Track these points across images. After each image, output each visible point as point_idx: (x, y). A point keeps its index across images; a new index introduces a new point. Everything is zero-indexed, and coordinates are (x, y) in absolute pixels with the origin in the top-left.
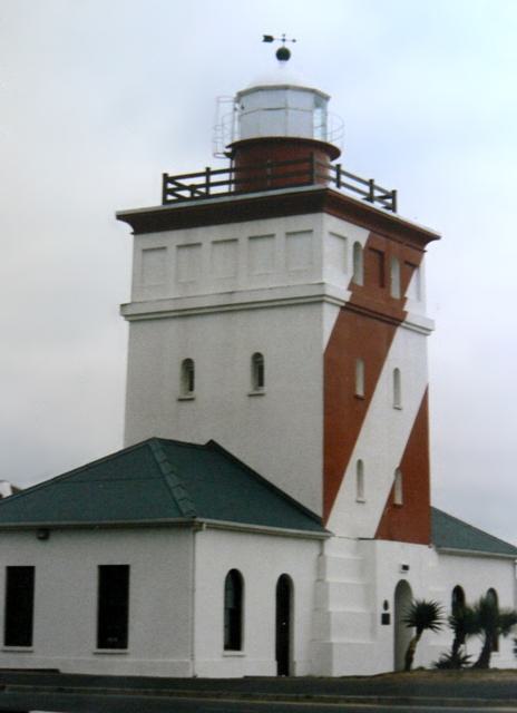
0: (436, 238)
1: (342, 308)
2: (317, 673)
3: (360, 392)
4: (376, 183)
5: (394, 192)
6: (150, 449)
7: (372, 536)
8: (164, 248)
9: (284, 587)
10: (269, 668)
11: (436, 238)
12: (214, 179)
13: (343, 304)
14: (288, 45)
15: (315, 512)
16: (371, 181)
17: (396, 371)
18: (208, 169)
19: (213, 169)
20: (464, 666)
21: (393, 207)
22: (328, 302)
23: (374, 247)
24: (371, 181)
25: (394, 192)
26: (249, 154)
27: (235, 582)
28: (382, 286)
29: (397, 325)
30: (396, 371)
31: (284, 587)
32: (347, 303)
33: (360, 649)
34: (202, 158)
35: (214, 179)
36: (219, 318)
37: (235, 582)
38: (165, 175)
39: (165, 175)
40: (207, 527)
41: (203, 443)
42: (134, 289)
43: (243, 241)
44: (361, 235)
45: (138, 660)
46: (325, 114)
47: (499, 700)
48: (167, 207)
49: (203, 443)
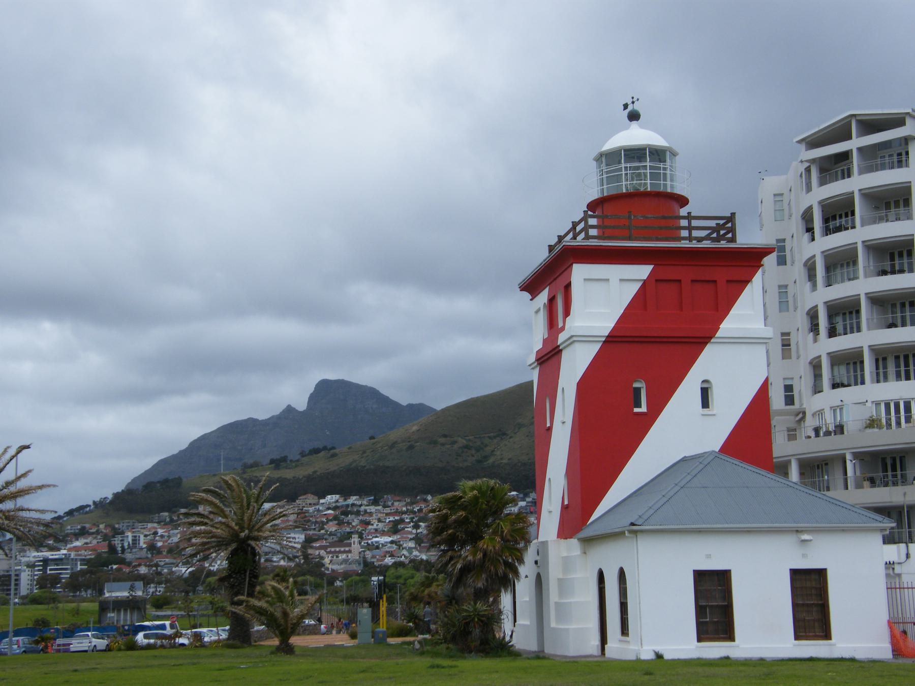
5: (733, 214)
8: (608, 280)
14: (637, 107)
21: (732, 230)
25: (733, 214)
35: (695, 223)
43: (614, 281)
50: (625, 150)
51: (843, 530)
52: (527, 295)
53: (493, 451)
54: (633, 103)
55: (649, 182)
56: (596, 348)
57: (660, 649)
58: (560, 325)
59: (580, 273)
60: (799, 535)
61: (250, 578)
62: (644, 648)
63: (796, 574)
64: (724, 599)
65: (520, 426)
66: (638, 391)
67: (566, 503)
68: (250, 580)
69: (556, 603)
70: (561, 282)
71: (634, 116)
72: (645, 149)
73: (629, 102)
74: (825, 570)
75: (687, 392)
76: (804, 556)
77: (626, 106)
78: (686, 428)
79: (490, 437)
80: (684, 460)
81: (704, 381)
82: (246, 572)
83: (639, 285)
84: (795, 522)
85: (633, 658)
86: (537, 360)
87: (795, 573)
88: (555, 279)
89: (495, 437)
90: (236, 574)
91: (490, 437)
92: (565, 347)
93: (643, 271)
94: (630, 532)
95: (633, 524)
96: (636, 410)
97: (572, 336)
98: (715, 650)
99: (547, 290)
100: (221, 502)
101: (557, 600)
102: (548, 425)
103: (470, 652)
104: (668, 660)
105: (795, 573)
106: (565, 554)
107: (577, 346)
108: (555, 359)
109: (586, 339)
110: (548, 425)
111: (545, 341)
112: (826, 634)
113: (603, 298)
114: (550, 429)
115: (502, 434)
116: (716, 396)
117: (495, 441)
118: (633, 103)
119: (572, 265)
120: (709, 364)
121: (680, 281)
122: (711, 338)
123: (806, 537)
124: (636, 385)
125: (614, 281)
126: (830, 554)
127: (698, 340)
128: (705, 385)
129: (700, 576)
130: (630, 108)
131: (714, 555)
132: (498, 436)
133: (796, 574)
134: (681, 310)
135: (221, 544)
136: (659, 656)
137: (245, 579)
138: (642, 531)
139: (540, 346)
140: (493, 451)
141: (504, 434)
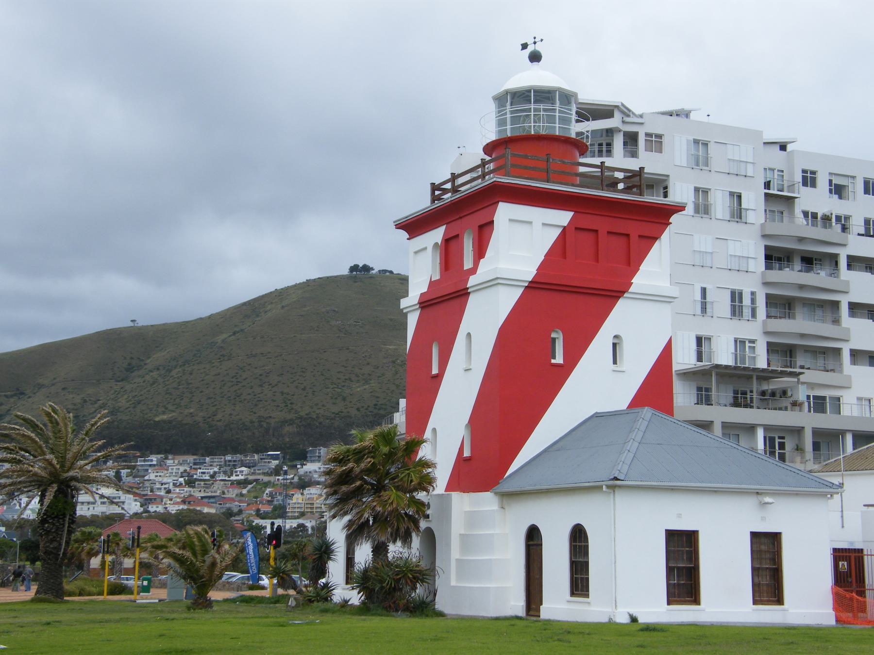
1: (526, 287)
3: (559, 359)
6: (759, 569)
8: (530, 223)
9: (578, 535)
10: (516, 605)
12: (460, 181)
14: (539, 47)
15: (420, 452)
17: (469, 335)
19: (457, 172)
22: (474, 291)
23: (769, 330)
27: (533, 536)
30: (469, 335)
31: (578, 535)
32: (530, 282)
33: (630, 588)
35: (460, 181)
37: (533, 536)
38: (433, 184)
39: (433, 184)
41: (344, 270)
43: (537, 225)
45: (594, 610)
46: (766, 178)
47: (781, 631)
48: (438, 204)
49: (426, 290)
50: (511, 93)
51: (797, 494)
52: (404, 234)
53: (9, 410)
54: (535, 43)
55: (557, 125)
56: (519, 292)
57: (635, 612)
58: (468, 264)
60: (760, 498)
61: (69, 523)
62: (620, 610)
63: (755, 536)
64: (690, 560)
65: (41, 386)
66: (554, 340)
67: (467, 453)
68: (69, 527)
69: (457, 560)
70: (480, 218)
71: (535, 57)
72: (529, 91)
73: (530, 41)
74: (780, 533)
75: (599, 347)
76: (763, 519)
77: (525, 46)
78: (597, 384)
79: (6, 396)
80: (597, 416)
81: (616, 337)
82: (65, 517)
83: (558, 231)
84: (758, 484)
85: (605, 619)
86: (420, 303)
87: (754, 535)
88: (461, 218)
89: (12, 396)
90: (53, 518)
91: (6, 396)
92: (474, 291)
93: (564, 217)
94: (608, 487)
95: (616, 479)
96: (553, 361)
97: (497, 278)
98: (684, 614)
99: (443, 228)
100: (37, 434)
101: (458, 557)
102: (435, 371)
103: (397, 611)
104: (549, 621)
105: (754, 535)
106: (468, 509)
107: (501, 289)
108: (455, 303)
109: (509, 283)
110: (435, 371)
111: (432, 284)
112: (779, 599)
113: (522, 242)
114: (439, 377)
115: (20, 393)
116: (627, 349)
117: (12, 400)
118: (535, 43)
119: (498, 202)
120: (622, 318)
121: (596, 231)
122: (624, 292)
123: (768, 499)
124: (553, 335)
125: (537, 225)
126: (787, 518)
127: (613, 293)
128: (616, 341)
129: (671, 535)
130: (531, 48)
131: (684, 514)
132: (15, 395)
133: (755, 536)
134: (597, 260)
135: (40, 484)
136: (634, 620)
137: (64, 525)
138: (620, 487)
139: (425, 289)
140: (9, 410)
141: (22, 393)
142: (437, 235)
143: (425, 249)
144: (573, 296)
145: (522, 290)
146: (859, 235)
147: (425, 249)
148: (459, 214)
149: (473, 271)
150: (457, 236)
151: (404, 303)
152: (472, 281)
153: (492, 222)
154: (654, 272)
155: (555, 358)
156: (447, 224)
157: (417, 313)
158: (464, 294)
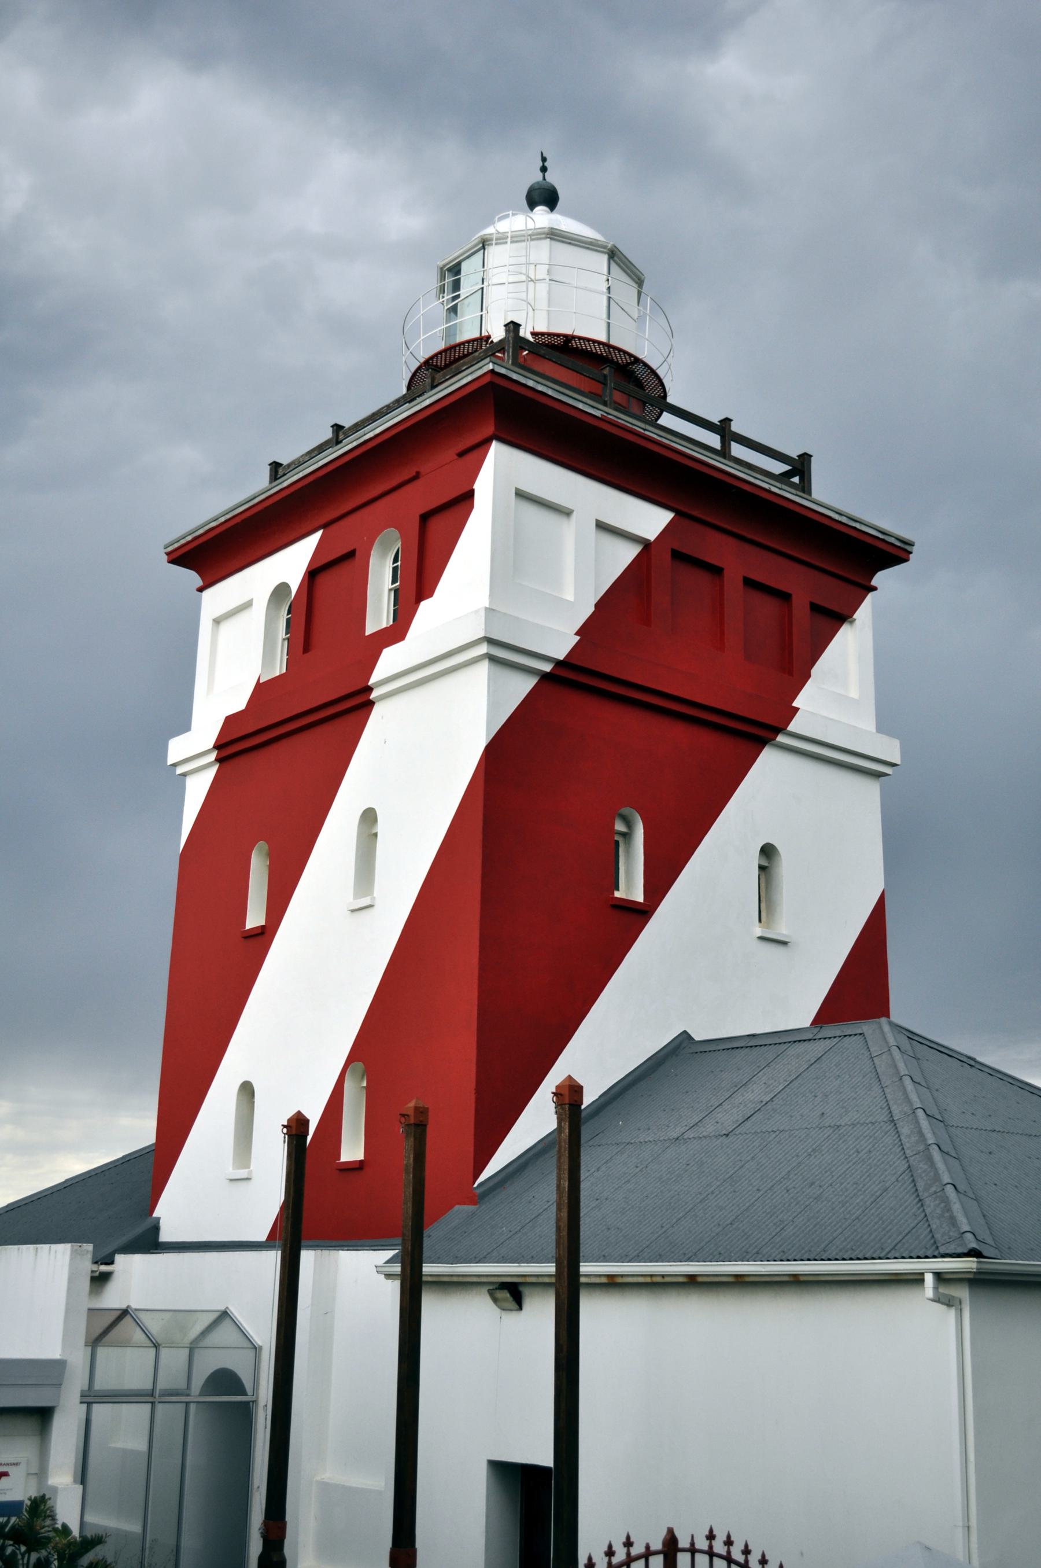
0: (891, 553)
1: (545, 677)
2: (326, 1252)
3: (632, 887)
4: (735, 427)
5: (805, 459)
7: (263, 1237)
11: (891, 553)
13: (547, 668)
16: (727, 421)
17: (369, 817)
18: (648, 1547)
20: (352, 1149)
21: (805, 487)
24: (727, 421)
25: (805, 459)
26: (518, 1301)
28: (591, 393)
29: (761, 743)
30: (369, 817)
32: (559, 664)
34: (614, 1549)
36: (84, 1417)
40: (512, 242)
42: (735, 433)
44: (308, 1258)
58: (379, 615)
59: (502, 471)
93: (651, 520)
102: (255, 918)
110: (255, 918)
111: (262, 690)
113: (534, 557)
119: (486, 443)
139: (239, 703)
142: (291, 563)
143: (248, 605)
144: (623, 749)
145: (529, 684)
146: (17, 1464)
147: (248, 605)
148: (374, 493)
149: (397, 632)
150: (351, 555)
151: (178, 749)
152: (390, 661)
153: (473, 491)
154: (840, 689)
155: (618, 890)
156: (325, 526)
157: (211, 774)
158: (356, 705)
